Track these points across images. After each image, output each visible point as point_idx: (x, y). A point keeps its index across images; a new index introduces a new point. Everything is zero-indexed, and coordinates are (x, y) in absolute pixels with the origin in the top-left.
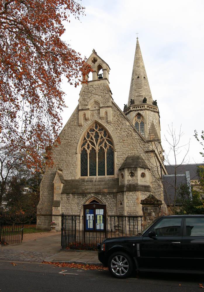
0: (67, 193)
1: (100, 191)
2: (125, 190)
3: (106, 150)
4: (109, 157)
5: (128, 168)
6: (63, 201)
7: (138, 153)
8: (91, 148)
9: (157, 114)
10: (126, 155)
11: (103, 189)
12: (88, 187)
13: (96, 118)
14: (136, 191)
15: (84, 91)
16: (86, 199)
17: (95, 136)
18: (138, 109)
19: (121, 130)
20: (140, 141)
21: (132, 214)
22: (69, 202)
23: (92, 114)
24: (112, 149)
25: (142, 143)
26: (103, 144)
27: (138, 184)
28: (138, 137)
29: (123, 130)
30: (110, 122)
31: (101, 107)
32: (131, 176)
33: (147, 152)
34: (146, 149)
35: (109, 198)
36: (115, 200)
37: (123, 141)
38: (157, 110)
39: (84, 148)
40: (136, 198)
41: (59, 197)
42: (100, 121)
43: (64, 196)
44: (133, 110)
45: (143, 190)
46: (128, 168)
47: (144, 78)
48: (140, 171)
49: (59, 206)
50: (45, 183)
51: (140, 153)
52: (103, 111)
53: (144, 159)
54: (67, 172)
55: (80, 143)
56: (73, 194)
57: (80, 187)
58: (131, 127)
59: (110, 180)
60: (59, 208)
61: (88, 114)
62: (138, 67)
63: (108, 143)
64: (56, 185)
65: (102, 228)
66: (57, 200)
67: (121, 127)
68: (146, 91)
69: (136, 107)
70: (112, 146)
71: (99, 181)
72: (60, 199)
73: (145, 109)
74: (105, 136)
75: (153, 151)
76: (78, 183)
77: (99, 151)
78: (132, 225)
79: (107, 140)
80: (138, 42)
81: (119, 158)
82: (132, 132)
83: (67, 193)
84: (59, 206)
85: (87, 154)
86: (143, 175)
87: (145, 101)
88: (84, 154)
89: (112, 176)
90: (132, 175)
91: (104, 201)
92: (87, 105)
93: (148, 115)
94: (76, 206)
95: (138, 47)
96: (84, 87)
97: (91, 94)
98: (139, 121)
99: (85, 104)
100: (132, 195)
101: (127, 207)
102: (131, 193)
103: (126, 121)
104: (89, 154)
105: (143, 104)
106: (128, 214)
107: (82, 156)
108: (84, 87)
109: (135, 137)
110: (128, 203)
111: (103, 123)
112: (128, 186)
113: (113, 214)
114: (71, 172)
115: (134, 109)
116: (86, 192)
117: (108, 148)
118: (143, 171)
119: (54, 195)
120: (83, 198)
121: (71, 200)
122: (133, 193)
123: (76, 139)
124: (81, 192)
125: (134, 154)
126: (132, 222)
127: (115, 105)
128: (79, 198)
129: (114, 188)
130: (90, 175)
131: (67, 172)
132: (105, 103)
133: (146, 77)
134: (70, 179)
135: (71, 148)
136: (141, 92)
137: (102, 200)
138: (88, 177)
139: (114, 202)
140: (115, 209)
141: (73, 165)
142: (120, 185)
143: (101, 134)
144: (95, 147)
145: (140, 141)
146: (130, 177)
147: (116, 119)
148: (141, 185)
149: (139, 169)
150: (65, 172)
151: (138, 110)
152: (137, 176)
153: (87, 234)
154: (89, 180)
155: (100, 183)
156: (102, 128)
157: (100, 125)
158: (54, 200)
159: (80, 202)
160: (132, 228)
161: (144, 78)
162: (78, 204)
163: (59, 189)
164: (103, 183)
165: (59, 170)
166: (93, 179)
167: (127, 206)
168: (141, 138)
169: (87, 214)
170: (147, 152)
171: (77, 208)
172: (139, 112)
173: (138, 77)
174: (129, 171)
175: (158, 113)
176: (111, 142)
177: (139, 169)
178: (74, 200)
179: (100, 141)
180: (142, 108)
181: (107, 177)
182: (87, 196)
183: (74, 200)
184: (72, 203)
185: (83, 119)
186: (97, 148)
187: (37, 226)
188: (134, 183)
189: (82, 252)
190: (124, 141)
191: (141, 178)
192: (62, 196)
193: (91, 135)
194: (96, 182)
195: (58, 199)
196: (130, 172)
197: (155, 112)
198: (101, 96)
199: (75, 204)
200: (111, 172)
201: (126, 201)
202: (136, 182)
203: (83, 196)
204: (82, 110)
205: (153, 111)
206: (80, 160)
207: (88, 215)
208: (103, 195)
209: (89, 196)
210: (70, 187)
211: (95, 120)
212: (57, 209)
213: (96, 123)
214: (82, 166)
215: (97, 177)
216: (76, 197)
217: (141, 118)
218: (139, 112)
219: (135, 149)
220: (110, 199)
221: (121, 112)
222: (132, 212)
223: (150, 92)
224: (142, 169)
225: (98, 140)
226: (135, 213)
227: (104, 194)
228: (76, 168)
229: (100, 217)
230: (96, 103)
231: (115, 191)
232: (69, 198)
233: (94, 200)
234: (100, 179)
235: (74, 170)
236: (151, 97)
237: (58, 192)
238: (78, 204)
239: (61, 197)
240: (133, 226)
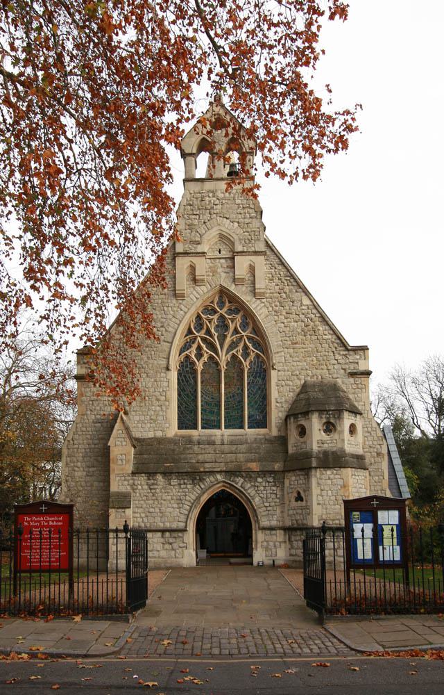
1: (240, 467)
2: (314, 464)
3: (246, 365)
4: (253, 382)
5: (321, 411)
6: (138, 494)
7: (330, 376)
8: (205, 358)
10: (300, 379)
11: (247, 461)
12: (205, 457)
13: (222, 280)
14: (340, 467)
15: (191, 203)
16: (203, 486)
17: (217, 326)
19: (288, 315)
20: (336, 345)
22: (153, 495)
23: (210, 268)
24: (263, 362)
25: (342, 353)
27: (344, 451)
28: (330, 337)
29: (294, 316)
30: (262, 294)
31: (237, 253)
32: (325, 431)
33: (352, 374)
34: (351, 368)
35: (264, 484)
37: (292, 344)
39: (187, 357)
40: (342, 483)
41: (126, 483)
42: (232, 288)
43: (142, 480)
45: (355, 466)
46: (321, 411)
48: (348, 419)
49: (130, 508)
50: (76, 446)
51: (335, 376)
52: (242, 263)
54: (143, 418)
55: (178, 341)
56: (167, 474)
57: (182, 456)
58: (314, 311)
59: (260, 439)
61: (202, 266)
64: (115, 452)
65: (369, 555)
67: (288, 308)
70: (261, 354)
71: (232, 443)
72: (129, 487)
74: (244, 325)
76: (176, 447)
77: (226, 366)
78: (330, 549)
79: (249, 338)
81: (282, 386)
82: (316, 323)
83: (149, 471)
84: (130, 508)
85: (195, 372)
88: (187, 373)
89: (262, 431)
90: (329, 428)
91: (249, 491)
92: (199, 243)
94: (175, 506)
96: (191, 194)
97: (210, 214)
99: (193, 239)
100: (332, 477)
102: (329, 472)
103: (303, 294)
108: (191, 194)
109: (324, 336)
110: (322, 496)
112: (321, 456)
113: (274, 523)
114: (152, 417)
116: (202, 470)
119: (112, 477)
120: (194, 484)
121: (161, 492)
122: (335, 472)
123: (166, 331)
124: (189, 470)
125: (320, 377)
126: (331, 541)
127: (273, 251)
129: (274, 461)
130: (202, 428)
131: (143, 418)
132: (247, 242)
134: (151, 435)
135: (151, 355)
137: (245, 490)
138: (198, 433)
139: (276, 494)
140: (278, 512)
141: (158, 400)
142: (293, 454)
143: (235, 322)
144: (217, 353)
145: (336, 348)
147: (277, 287)
149: (346, 414)
150: (137, 418)
152: (342, 432)
153: (357, 576)
154: (204, 438)
155: (235, 446)
156: (238, 307)
157: (233, 299)
158: (111, 490)
160: (331, 556)
163: (124, 462)
164: (243, 447)
167: (319, 504)
169: (354, 525)
170: (352, 374)
171: (178, 510)
174: (321, 418)
177: (346, 414)
178: (170, 491)
179: (232, 340)
181: (250, 433)
182: (204, 479)
183: (170, 491)
185: (187, 280)
186: (223, 359)
187: (259, 556)
188: (335, 449)
189: (388, 619)
190: (296, 344)
192: (134, 480)
193: (208, 324)
194: (223, 444)
195: (123, 489)
196: (324, 420)
198: (238, 222)
199: (172, 502)
200: (260, 421)
201: (315, 491)
202: (339, 445)
204: (186, 254)
207: (357, 527)
208: (247, 477)
210: (155, 457)
211: (221, 286)
212: (123, 514)
213: (223, 293)
214: (182, 404)
215: (223, 433)
219: (322, 367)
220: (265, 487)
221: (288, 271)
222: (332, 518)
225: (225, 337)
226: (338, 519)
227: (249, 475)
229: (392, 530)
230: (224, 238)
231: (277, 466)
232: (153, 484)
234: (233, 438)
235: (161, 413)
237: (123, 469)
239: (131, 482)
240: (332, 551)
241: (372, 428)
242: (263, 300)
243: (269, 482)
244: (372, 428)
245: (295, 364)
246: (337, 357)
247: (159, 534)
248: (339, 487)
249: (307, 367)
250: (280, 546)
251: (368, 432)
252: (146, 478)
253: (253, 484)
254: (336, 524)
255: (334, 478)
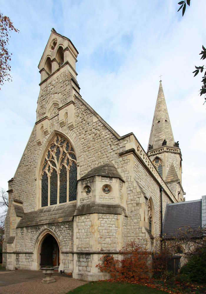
0: (21, 227)
9: (178, 156)
11: (59, 218)
18: (156, 153)
20: (112, 140)
21: (84, 249)
22: (23, 237)
26: (66, 161)
27: (94, 203)
28: (108, 136)
33: (121, 155)
36: (71, 231)
38: (179, 152)
42: (60, 130)
43: (19, 230)
44: (151, 155)
45: (103, 212)
47: (166, 121)
53: (116, 167)
56: (27, 227)
58: (100, 124)
60: (12, 244)
62: (159, 111)
63: (71, 158)
66: (13, 236)
68: (167, 134)
69: (154, 151)
72: (15, 234)
73: (164, 152)
75: (132, 151)
80: (161, 85)
82: (101, 131)
86: (107, 189)
87: (165, 143)
91: (57, 233)
93: (168, 158)
94: (30, 242)
95: (161, 90)
98: (157, 165)
100: (85, 220)
101: (78, 239)
102: (83, 218)
104: (51, 178)
105: (163, 146)
106: (79, 249)
107: (43, 182)
111: (64, 131)
115: (152, 154)
116: (39, 224)
117: (71, 165)
118: (107, 181)
122: (86, 217)
128: (32, 232)
133: (167, 120)
134: (30, 211)
136: (160, 137)
137: (56, 233)
139: (69, 234)
140: (70, 244)
141: (32, 195)
146: (85, 194)
148: (102, 203)
151: (156, 154)
156: (64, 139)
159: (33, 237)
161: (166, 121)
162: (31, 239)
165: (14, 201)
166: (51, 208)
167: (77, 238)
168: (114, 135)
170: (121, 155)
172: (158, 155)
173: (159, 122)
174: (83, 184)
175: (180, 154)
176: (74, 156)
180: (161, 151)
184: (26, 238)
188: (89, 203)
190: (89, 148)
191: (103, 192)
196: (84, 185)
197: (175, 153)
202: (92, 200)
203: (36, 229)
205: (173, 153)
206: (41, 187)
209: (42, 228)
211: (55, 131)
213: (57, 134)
216: (29, 231)
217: (159, 161)
218: (158, 155)
219: (104, 156)
223: (172, 135)
224: (106, 178)
226: (88, 248)
228: (35, 198)
230: (55, 104)
233: (48, 233)
236: (172, 139)
238: (31, 239)
241: (133, 187)
242: (73, 130)
243: (66, 228)
244: (133, 187)
245: (89, 159)
246: (113, 147)
247: (24, 255)
248: (89, 227)
249: (95, 159)
250: (71, 262)
251: (131, 190)
252: (20, 230)
253: (59, 229)
254: (86, 251)
255: (86, 221)
